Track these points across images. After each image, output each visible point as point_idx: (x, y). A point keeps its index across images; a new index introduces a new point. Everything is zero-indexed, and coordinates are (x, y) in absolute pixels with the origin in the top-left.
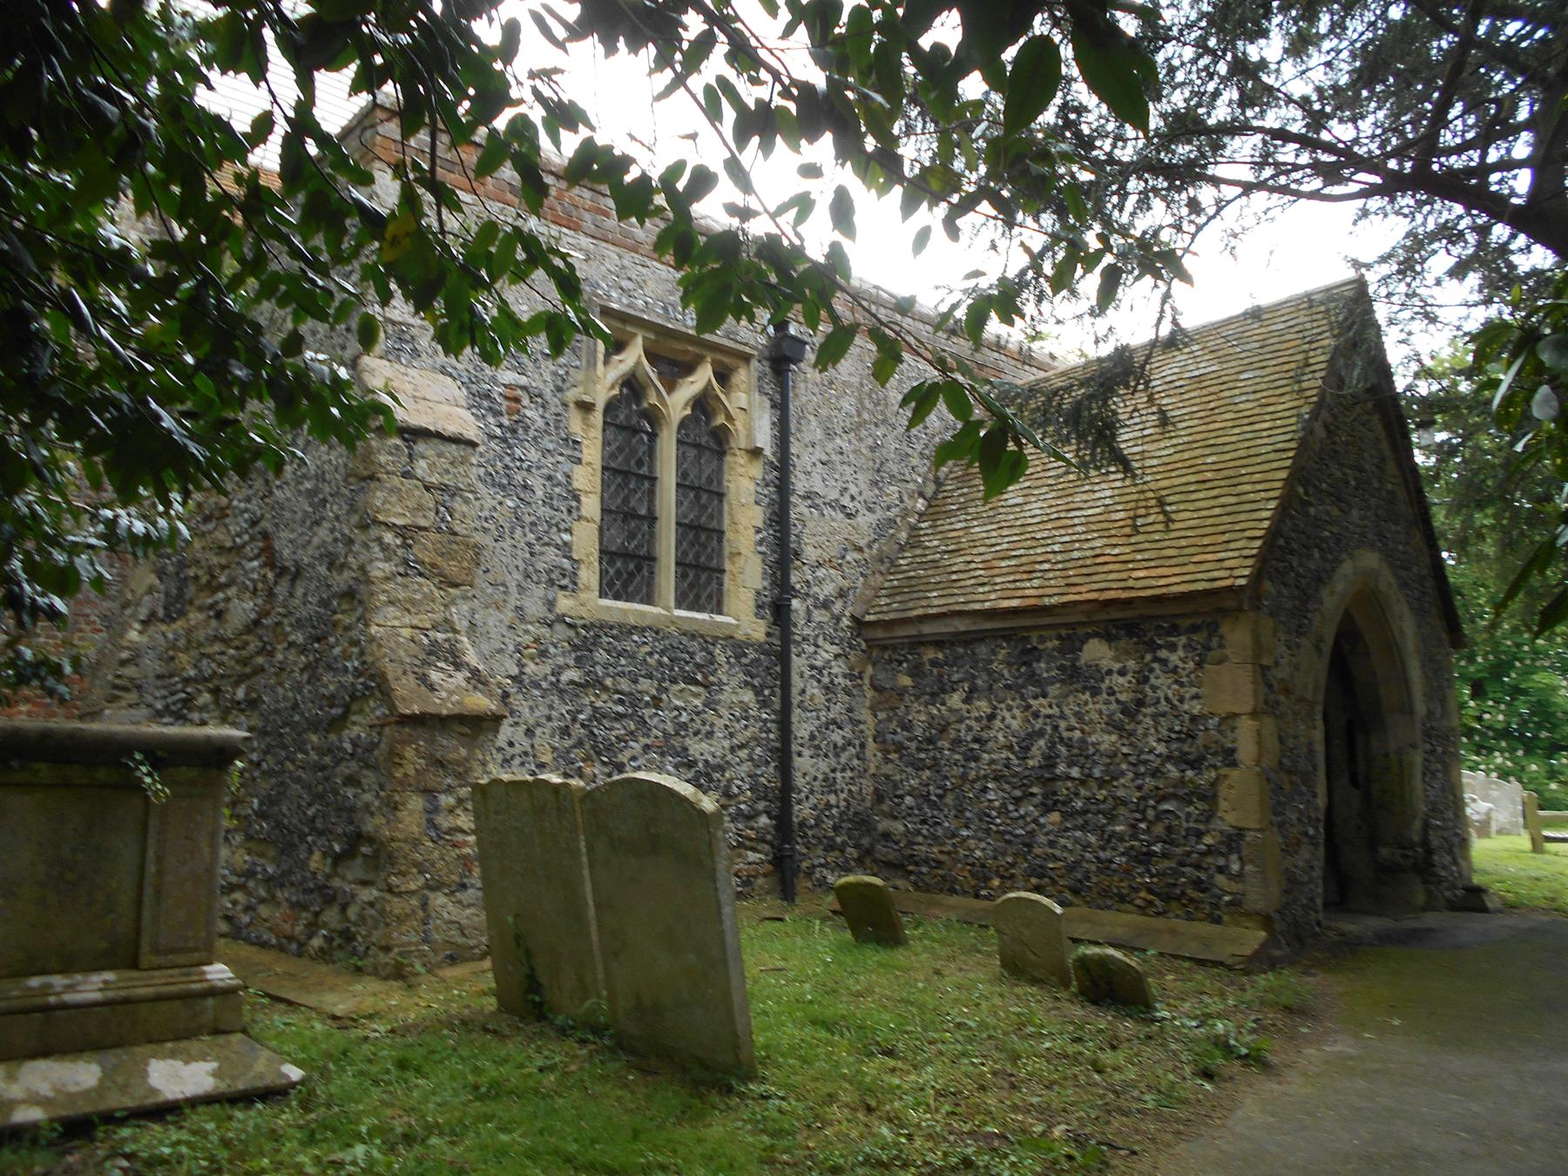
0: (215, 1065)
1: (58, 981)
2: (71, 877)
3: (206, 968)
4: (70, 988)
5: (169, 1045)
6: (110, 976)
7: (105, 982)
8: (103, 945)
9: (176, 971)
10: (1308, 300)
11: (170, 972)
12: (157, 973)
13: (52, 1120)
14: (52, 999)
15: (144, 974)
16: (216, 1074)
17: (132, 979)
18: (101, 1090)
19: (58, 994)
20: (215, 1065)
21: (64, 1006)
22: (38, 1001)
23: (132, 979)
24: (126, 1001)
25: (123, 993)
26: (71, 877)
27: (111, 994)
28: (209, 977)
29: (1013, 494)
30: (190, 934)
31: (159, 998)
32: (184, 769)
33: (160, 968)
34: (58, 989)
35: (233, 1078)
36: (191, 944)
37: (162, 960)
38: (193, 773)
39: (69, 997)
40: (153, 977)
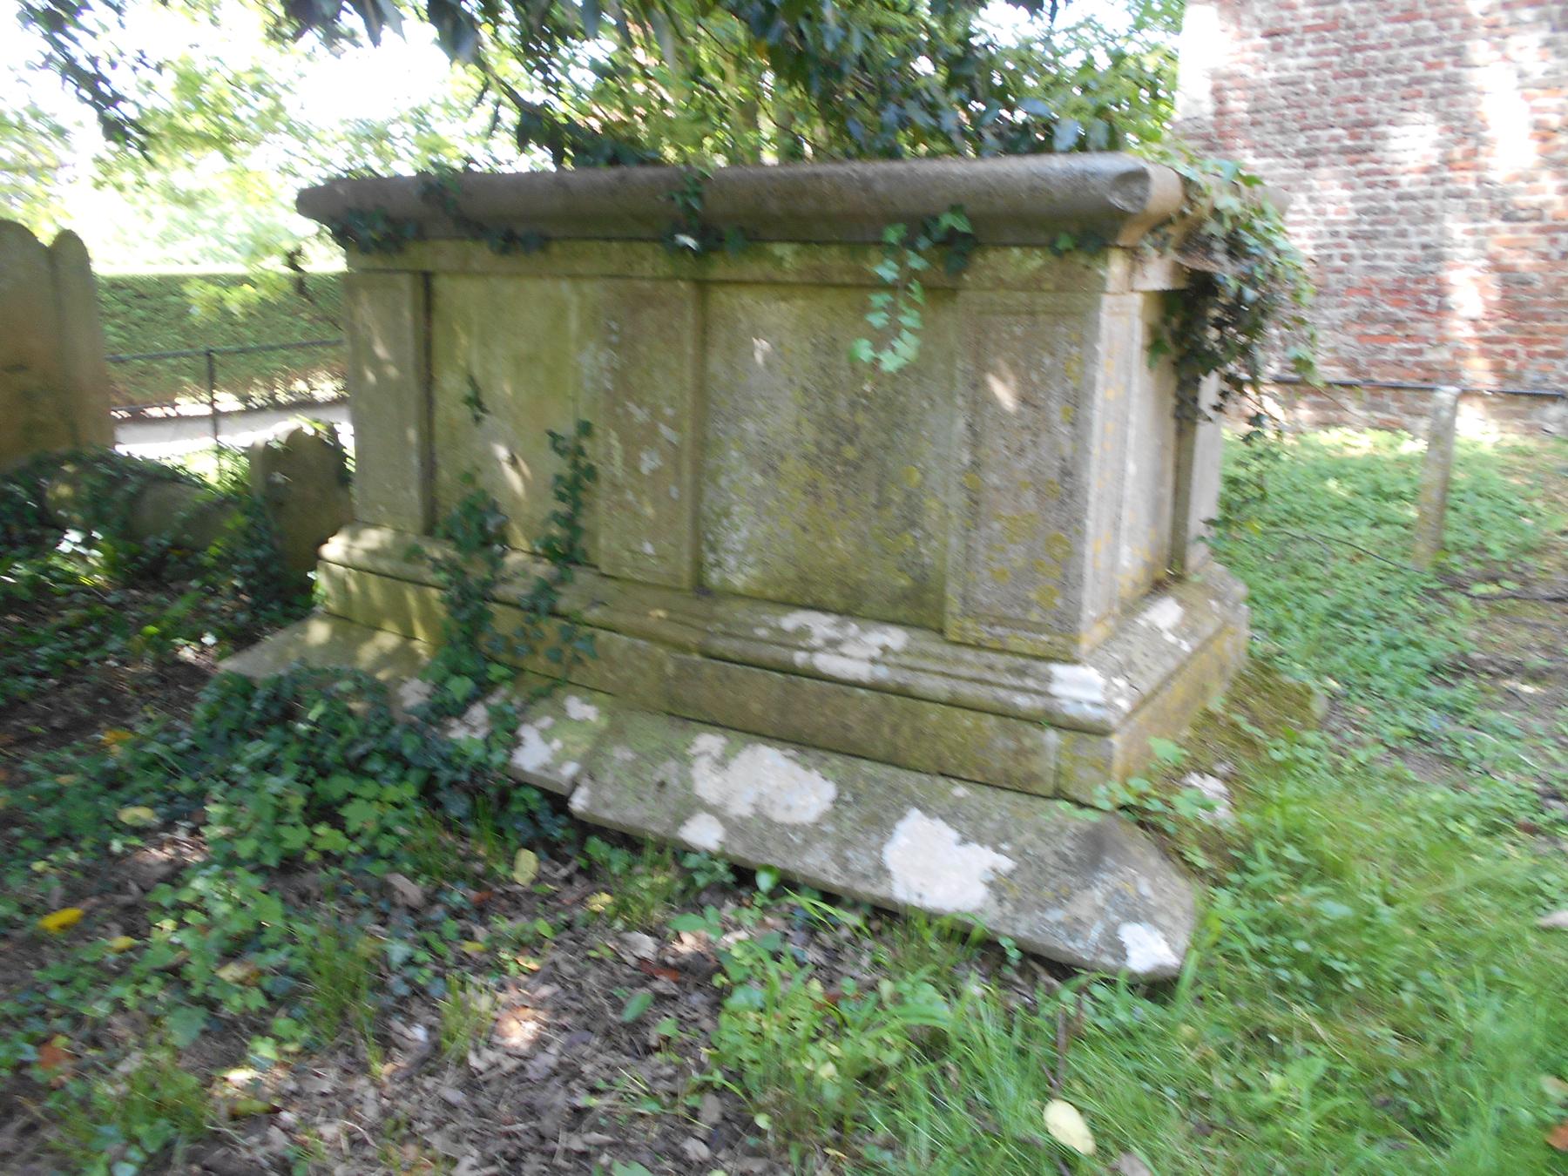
0: (1006, 864)
1: (821, 626)
2: (850, 452)
3: (1058, 670)
4: (833, 644)
5: (960, 791)
6: (896, 638)
7: (885, 649)
8: (904, 582)
9: (1001, 661)
10: (1150, 366)
11: (992, 657)
12: (969, 655)
13: (722, 855)
14: (800, 658)
15: (948, 651)
16: (998, 886)
17: (924, 655)
18: (812, 833)
19: (812, 650)
20: (1006, 864)
21: (815, 675)
22: (780, 653)
23: (924, 655)
24: (903, 692)
25: (902, 677)
26: (850, 452)
27: (882, 673)
28: (1055, 689)
29: (201, 69)
30: (1033, 596)
31: (954, 703)
32: (1016, 252)
33: (978, 646)
34: (817, 642)
35: (1019, 905)
36: (1034, 616)
37: (982, 633)
38: (1036, 261)
39: (827, 663)
40: (958, 661)
